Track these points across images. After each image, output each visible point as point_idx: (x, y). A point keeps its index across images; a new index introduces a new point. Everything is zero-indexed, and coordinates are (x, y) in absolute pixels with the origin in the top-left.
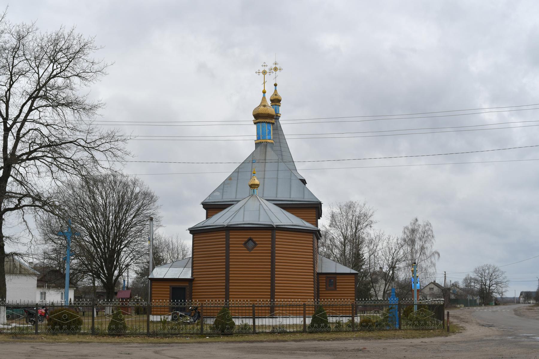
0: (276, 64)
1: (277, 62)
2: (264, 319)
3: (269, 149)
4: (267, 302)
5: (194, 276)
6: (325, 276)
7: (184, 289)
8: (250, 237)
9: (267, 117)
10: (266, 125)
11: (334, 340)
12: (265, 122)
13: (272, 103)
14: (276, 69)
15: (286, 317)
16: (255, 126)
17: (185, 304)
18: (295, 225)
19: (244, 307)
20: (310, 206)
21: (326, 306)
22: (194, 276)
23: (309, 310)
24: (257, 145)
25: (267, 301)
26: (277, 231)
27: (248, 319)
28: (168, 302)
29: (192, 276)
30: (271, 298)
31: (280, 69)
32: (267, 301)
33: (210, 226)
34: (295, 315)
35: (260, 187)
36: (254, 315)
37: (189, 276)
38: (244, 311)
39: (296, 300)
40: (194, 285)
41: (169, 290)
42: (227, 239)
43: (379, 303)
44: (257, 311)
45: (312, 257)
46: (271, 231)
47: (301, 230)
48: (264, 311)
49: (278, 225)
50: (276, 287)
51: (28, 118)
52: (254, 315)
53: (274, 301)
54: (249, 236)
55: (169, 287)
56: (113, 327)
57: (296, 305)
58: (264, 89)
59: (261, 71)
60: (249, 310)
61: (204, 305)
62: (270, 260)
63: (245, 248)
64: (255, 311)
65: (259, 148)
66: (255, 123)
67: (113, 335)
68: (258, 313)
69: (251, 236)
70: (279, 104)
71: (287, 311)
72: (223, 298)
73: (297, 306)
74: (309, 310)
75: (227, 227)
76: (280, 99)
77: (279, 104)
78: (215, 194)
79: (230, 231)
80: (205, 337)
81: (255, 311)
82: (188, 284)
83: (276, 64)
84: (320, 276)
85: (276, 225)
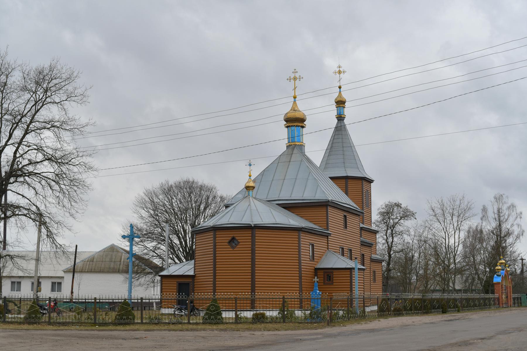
0: (339, 67)
1: (341, 65)
2: (246, 312)
3: (295, 151)
4: (248, 295)
5: (196, 273)
6: (322, 271)
7: (188, 284)
8: (233, 236)
9: (295, 120)
10: (295, 128)
11: (102, 331)
12: (295, 126)
13: (337, 105)
14: (340, 72)
15: (269, 311)
16: (286, 129)
17: (182, 297)
18: (276, 224)
19: (274, 299)
20: (319, 204)
21: (220, 299)
22: (196, 273)
23: (240, 303)
24: (288, 147)
25: (173, 294)
26: (256, 230)
27: (231, 312)
28: (250, 295)
29: (194, 273)
30: (252, 293)
31: (344, 72)
32: (173, 294)
33: (281, 224)
34: (278, 309)
35: (255, 190)
36: (236, 308)
37: (191, 273)
38: (275, 302)
39: (240, 294)
40: (195, 281)
41: (176, 285)
42: (253, 237)
43: (184, 297)
44: (239, 304)
45: (297, 253)
46: (251, 230)
47: (283, 228)
48: (294, 302)
49: (256, 224)
50: (256, 282)
51: (23, 141)
52: (236, 308)
53: (254, 294)
54: (233, 235)
55: (176, 283)
56: (259, 316)
57: (229, 299)
58: (295, 95)
59: (292, 78)
60: (279, 301)
61: (285, 297)
62: (250, 257)
63: (229, 247)
64: (238, 304)
65: (288, 150)
66: (287, 127)
67: (30, 323)
68: (240, 306)
69: (234, 235)
70: (344, 106)
71: (270, 305)
72: (174, 292)
73: (229, 299)
74: (240, 303)
75: (212, 227)
76: (344, 100)
77: (344, 106)
78: (237, 196)
79: (217, 231)
80: (95, 326)
81: (238, 304)
82: (191, 280)
83: (339, 67)
84: (318, 271)
85: (254, 224)
